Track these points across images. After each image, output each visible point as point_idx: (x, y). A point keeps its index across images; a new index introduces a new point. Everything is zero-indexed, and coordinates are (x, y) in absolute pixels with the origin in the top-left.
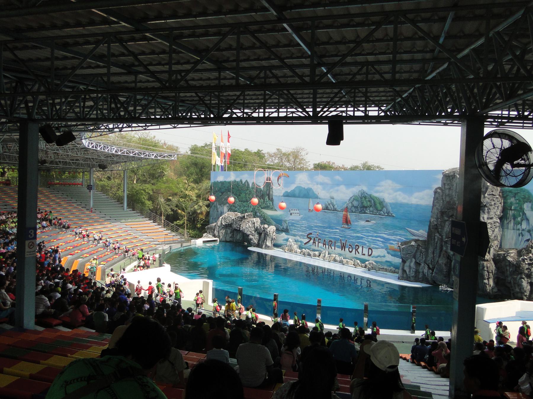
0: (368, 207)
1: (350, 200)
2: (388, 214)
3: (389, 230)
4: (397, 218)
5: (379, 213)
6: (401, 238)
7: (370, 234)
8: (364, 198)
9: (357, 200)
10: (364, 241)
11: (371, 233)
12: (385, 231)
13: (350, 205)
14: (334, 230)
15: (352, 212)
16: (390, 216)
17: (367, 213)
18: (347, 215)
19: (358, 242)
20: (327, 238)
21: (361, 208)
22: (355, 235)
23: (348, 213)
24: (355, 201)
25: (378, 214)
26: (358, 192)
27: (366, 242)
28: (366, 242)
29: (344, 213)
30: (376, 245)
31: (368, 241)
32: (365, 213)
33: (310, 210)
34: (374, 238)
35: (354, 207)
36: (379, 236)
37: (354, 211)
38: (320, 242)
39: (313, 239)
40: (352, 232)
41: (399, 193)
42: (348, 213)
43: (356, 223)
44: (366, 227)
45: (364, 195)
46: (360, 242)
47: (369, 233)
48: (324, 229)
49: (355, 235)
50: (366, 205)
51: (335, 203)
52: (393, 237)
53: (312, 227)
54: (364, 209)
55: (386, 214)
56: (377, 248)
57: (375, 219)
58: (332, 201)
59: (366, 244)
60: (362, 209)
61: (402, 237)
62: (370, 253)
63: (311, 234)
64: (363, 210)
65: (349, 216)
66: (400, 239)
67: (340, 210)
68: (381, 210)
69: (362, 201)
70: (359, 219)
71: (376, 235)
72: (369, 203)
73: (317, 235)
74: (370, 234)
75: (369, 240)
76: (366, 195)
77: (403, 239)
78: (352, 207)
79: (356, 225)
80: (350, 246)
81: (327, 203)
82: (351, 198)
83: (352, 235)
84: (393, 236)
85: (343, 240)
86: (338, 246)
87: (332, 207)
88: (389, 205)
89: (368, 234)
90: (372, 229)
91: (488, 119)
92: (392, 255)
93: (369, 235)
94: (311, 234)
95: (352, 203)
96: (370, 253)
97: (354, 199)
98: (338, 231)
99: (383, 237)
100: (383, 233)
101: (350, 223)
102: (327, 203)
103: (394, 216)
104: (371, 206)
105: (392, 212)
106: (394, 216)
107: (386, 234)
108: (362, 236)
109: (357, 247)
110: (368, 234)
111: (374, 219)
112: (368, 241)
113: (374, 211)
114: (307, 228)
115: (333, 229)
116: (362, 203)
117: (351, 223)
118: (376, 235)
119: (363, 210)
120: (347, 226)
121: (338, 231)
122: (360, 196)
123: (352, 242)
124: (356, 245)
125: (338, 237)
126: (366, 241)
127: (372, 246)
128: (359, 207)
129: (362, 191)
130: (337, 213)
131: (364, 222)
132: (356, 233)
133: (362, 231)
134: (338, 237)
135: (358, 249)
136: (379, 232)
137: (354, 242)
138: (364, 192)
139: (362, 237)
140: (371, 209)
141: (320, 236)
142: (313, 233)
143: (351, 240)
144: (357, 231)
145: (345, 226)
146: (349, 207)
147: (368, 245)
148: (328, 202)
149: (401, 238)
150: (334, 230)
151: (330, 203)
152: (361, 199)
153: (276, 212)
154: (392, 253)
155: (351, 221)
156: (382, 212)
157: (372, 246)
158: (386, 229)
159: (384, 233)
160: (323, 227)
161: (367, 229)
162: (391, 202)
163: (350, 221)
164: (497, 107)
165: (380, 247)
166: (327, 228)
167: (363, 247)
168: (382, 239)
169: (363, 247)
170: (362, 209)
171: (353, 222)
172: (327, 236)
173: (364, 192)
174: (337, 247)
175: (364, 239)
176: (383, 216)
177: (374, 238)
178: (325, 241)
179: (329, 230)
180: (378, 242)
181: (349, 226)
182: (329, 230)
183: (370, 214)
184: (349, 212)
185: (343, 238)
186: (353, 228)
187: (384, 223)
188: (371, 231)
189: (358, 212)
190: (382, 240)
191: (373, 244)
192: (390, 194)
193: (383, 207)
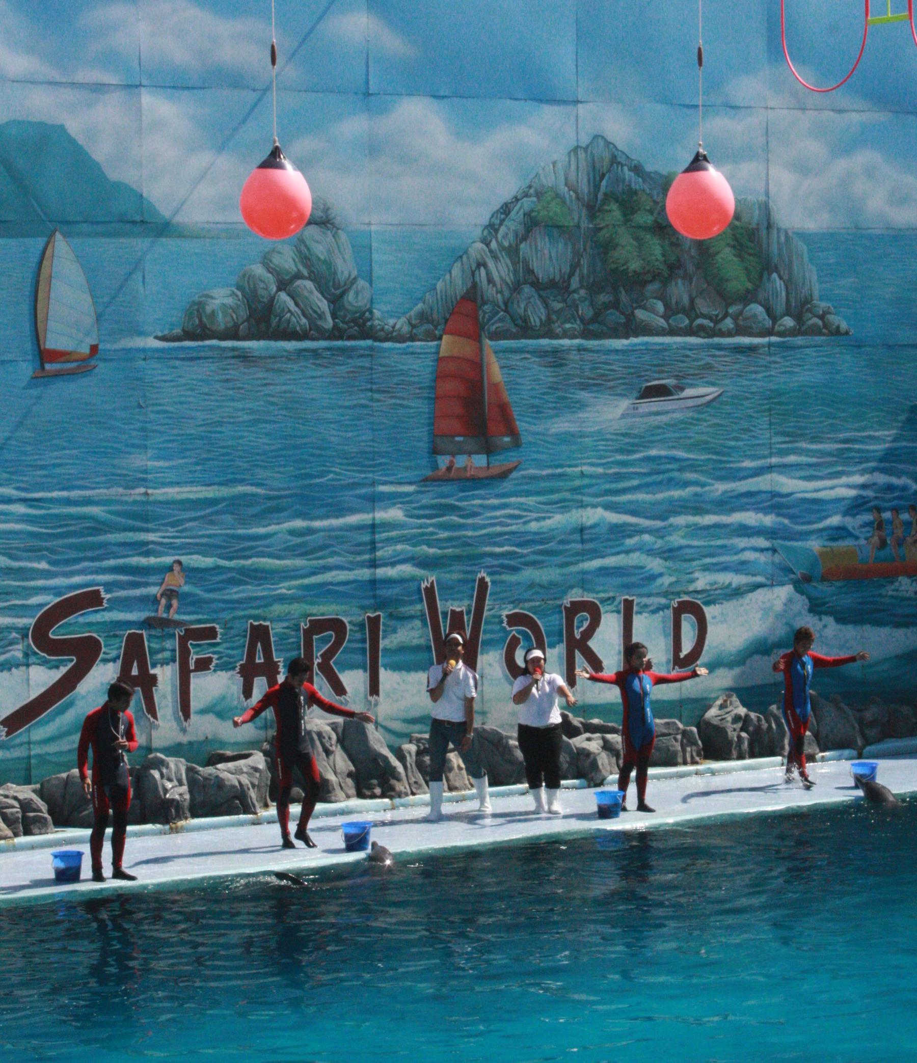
0: (656, 276)
1: (492, 228)
2: (799, 318)
3: (814, 439)
4: (858, 345)
5: (735, 318)
6: (894, 480)
7: (677, 493)
8: (615, 212)
9: (556, 228)
10: (635, 559)
11: (686, 484)
12: (783, 453)
13: (501, 270)
14: (353, 519)
15: (525, 330)
16: (814, 331)
17: (647, 330)
18: (478, 365)
19: (584, 581)
20: (278, 609)
21: (594, 288)
22: (558, 520)
23: (488, 343)
24: (537, 232)
25: (729, 323)
26: (560, 154)
27: (655, 565)
28: (655, 565)
29: (447, 345)
30: (725, 568)
31: (669, 554)
32: (631, 328)
33: (45, 356)
34: (709, 519)
35: (536, 285)
36: (749, 494)
37: (535, 321)
38: (203, 665)
39: (112, 648)
40: (531, 501)
41: (864, 157)
42: (488, 343)
43: (562, 425)
44: (647, 445)
45: (619, 180)
46: (604, 571)
47: (671, 483)
48: (244, 522)
49: (558, 520)
50: (635, 265)
51: (345, 267)
52: (844, 480)
53: (100, 527)
54: (624, 297)
55: (788, 322)
56: (736, 593)
57: (708, 367)
58: (319, 250)
59: (653, 578)
60: (604, 298)
61: (899, 474)
62: (687, 647)
63: (91, 600)
64: (615, 305)
65: (496, 371)
66: (890, 488)
67: (402, 325)
68: (748, 297)
69: (604, 235)
70: (585, 387)
71: (721, 487)
72: (656, 248)
73: (170, 594)
74: (677, 493)
75: (676, 540)
76: (637, 183)
77: (904, 488)
78: (516, 288)
79: (565, 438)
80: (514, 631)
81: (259, 270)
82: (506, 209)
83: (534, 526)
84: (838, 474)
85: (444, 587)
86: (402, 649)
87: (323, 305)
88: (803, 247)
89: (660, 496)
90: (690, 448)
91: (94, 752)
92: (841, 619)
93: (671, 501)
94: (91, 600)
95: (513, 252)
96: (687, 647)
97: (531, 223)
98: (395, 514)
99: (774, 494)
100: (770, 468)
101: (513, 432)
102: (259, 270)
103: (844, 326)
104: (674, 268)
105: (823, 305)
106: (837, 332)
107: (798, 466)
108: (614, 518)
109: (582, 622)
110: (660, 496)
111: (705, 372)
112: (669, 554)
113: (703, 306)
114: (34, 552)
115: (341, 511)
116: (606, 247)
117: (521, 425)
118: (721, 487)
119: (615, 305)
120: (480, 460)
121: (395, 514)
122: (584, 188)
123: (532, 585)
124: (576, 607)
125: (406, 569)
126: (651, 552)
127: (702, 581)
128: (575, 283)
129: (600, 151)
130: (371, 353)
131: (624, 404)
132: (564, 506)
133: (618, 477)
134: (406, 569)
135: (589, 633)
136: (748, 464)
137: (552, 584)
138: (614, 160)
139: (619, 532)
140: (679, 291)
141: (193, 603)
142: (109, 587)
143: (528, 574)
144: (575, 490)
145: (461, 461)
146: (490, 292)
147: (667, 580)
148: (266, 261)
149: (894, 480)
150: (353, 519)
151: (287, 260)
152: (592, 217)
153: (259, 163)
154: (847, 601)
155: (515, 411)
156: (757, 309)
157: (700, 585)
158: (794, 436)
159: (783, 468)
160: (234, 505)
161: (654, 452)
162: (811, 225)
163: (504, 410)
164: (653, 418)
165: (760, 579)
166: (279, 510)
167: (628, 605)
168: (765, 511)
169: (628, 605)
170: (604, 298)
171: (537, 412)
172: (283, 588)
173: (614, 160)
174: (396, 667)
175: (630, 542)
176: (762, 334)
177: (709, 519)
178: (260, 634)
179: (299, 524)
180: (741, 542)
181: (501, 461)
182: (299, 524)
183: (672, 332)
184: (495, 336)
185: (452, 576)
186: (540, 465)
187: (779, 393)
188: (693, 467)
189: (577, 326)
190: (768, 520)
191: (706, 568)
192: (802, 168)
193: (767, 267)
